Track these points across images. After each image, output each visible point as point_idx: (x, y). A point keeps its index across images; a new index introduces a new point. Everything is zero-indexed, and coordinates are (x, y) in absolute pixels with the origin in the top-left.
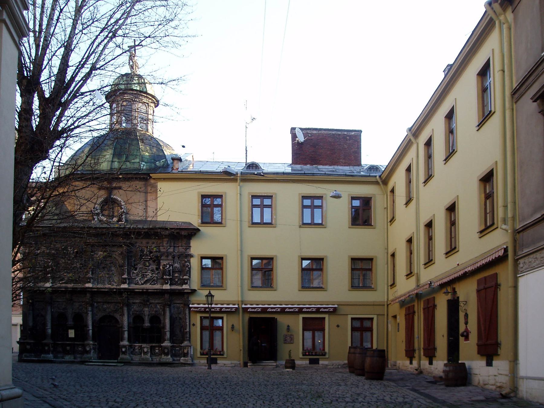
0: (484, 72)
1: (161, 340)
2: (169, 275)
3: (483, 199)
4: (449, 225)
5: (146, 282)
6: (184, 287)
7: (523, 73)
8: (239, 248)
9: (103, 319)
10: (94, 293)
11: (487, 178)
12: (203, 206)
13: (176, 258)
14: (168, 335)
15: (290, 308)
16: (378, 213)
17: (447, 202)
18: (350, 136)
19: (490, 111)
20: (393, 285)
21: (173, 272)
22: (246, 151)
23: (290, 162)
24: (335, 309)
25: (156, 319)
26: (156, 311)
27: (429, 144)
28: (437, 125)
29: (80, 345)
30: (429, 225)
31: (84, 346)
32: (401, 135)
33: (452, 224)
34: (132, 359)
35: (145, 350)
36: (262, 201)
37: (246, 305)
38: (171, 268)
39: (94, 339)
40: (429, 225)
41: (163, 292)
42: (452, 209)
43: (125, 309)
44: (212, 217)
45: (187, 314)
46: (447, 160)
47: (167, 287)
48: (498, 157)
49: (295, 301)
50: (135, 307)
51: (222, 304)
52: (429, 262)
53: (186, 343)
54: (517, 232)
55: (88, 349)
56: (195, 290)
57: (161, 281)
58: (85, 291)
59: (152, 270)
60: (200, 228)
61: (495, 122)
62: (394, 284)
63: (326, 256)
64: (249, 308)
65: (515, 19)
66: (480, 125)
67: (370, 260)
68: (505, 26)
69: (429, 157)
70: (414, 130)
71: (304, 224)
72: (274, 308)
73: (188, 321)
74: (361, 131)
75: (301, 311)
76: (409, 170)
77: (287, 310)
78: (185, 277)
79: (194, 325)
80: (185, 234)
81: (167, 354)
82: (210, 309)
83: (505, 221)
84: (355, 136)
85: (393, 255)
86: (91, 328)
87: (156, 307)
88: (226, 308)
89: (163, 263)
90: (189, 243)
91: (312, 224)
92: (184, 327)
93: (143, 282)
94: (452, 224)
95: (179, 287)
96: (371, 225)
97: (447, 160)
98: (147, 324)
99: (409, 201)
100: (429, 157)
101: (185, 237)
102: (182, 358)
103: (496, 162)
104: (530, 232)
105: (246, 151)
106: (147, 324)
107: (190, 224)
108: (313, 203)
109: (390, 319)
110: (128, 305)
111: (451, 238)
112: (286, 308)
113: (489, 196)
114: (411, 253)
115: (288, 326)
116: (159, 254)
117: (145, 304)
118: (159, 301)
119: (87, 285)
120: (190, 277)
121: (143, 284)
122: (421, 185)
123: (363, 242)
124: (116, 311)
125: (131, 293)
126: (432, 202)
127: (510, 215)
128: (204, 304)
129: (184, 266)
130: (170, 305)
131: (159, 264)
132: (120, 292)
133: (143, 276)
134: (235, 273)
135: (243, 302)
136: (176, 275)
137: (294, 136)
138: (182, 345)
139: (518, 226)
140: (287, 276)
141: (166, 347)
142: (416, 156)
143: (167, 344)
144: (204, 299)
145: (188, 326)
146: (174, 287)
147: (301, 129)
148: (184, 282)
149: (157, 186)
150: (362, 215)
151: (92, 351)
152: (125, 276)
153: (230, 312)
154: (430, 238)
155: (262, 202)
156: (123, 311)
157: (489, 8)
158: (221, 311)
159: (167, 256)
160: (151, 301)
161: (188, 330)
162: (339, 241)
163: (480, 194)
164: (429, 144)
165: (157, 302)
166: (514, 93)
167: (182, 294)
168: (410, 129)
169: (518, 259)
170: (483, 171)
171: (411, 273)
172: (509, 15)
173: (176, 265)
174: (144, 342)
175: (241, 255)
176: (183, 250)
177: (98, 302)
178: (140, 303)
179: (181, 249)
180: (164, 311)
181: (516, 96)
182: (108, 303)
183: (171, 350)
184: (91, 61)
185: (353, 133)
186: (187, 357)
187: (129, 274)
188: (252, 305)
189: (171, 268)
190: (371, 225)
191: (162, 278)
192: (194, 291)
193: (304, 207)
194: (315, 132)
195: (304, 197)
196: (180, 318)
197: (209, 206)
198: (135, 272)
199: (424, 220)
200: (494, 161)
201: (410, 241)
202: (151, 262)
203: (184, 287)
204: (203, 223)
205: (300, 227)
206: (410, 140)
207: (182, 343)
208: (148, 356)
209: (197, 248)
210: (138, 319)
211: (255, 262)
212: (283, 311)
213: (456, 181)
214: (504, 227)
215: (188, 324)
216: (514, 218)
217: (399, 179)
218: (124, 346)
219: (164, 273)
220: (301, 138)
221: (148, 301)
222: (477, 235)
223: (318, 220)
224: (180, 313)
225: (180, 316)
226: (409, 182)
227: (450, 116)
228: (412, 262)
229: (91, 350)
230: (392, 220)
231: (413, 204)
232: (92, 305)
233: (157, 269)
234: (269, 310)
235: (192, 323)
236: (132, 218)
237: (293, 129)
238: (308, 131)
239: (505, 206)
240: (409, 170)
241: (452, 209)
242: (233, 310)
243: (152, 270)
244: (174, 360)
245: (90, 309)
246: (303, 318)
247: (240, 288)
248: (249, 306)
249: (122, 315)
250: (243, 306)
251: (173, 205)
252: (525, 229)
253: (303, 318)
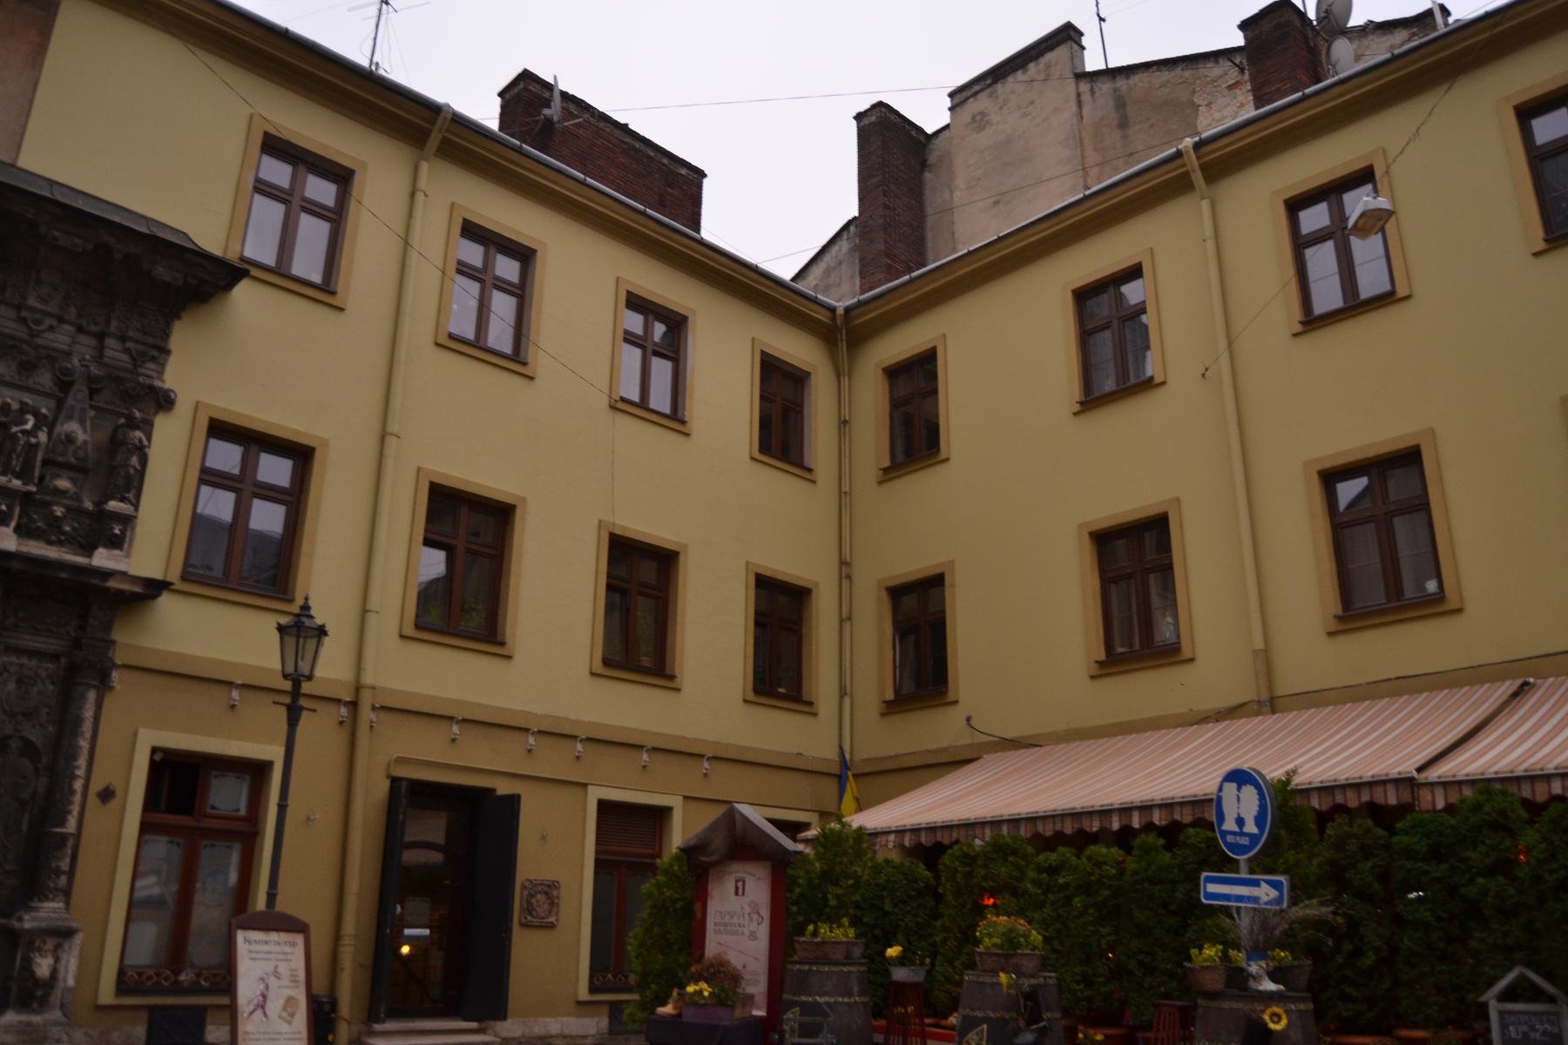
6: (102, 558)
13: (78, 395)
21: (45, 462)
38: (43, 437)
53: (49, 911)
80: (171, 281)
90: (166, 334)
109: (93, 800)
136: (63, 484)
145: (77, 798)
159: (27, 367)
173: (73, 427)
185: (684, 171)
186: (44, 1003)
193: (1301, 243)
195: (1295, 206)
203: (102, 558)
209: (231, 364)
211: (1348, 490)
223: (1371, 281)
228: (1481, 735)
235: (97, 785)
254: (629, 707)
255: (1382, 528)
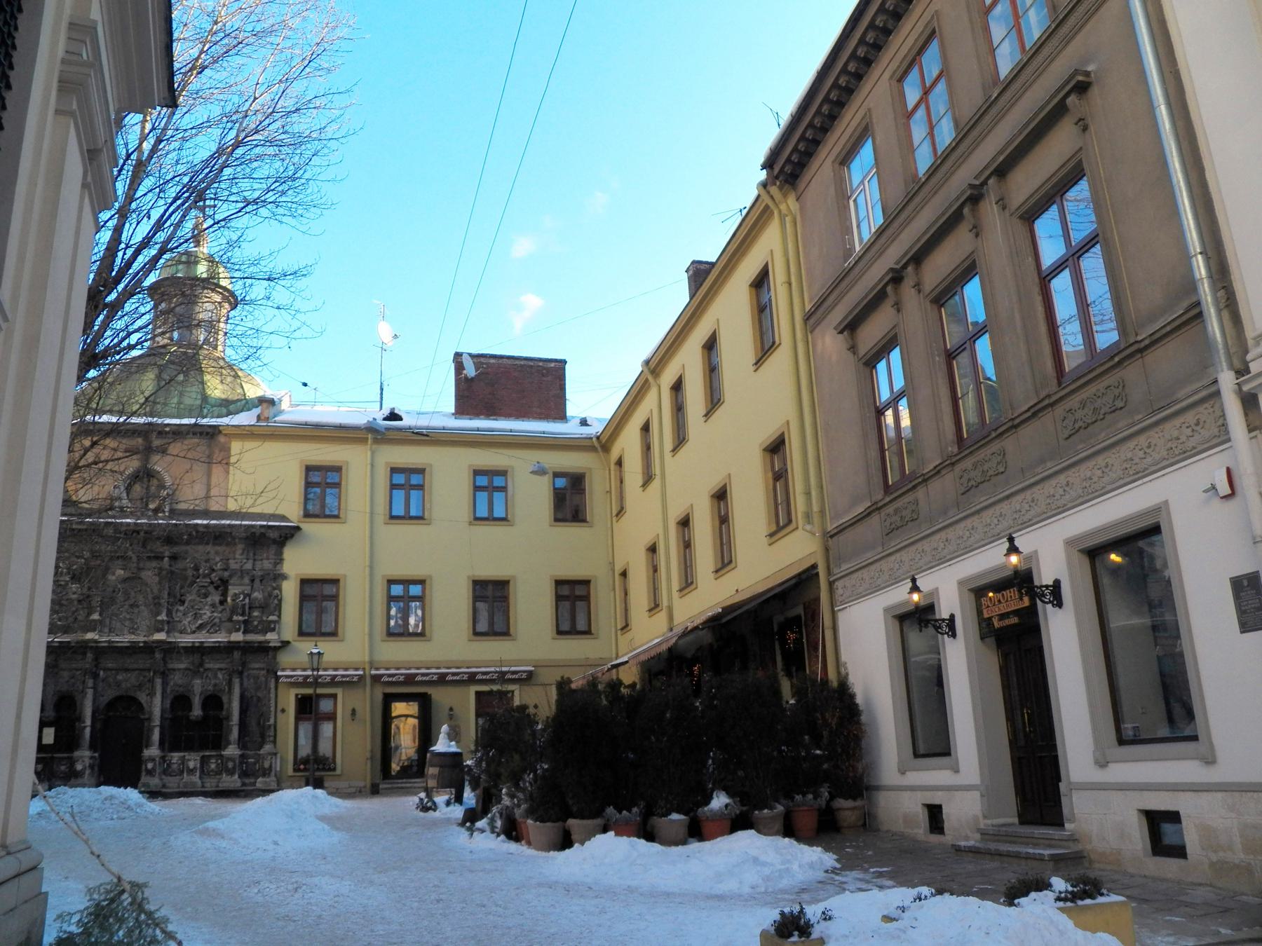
0: (761, 281)
1: (218, 743)
2: (243, 614)
3: (771, 482)
4: (717, 523)
5: (200, 627)
6: (270, 636)
7: (819, 291)
8: (367, 563)
9: (111, 705)
10: (100, 652)
11: (776, 447)
12: (308, 485)
13: (257, 582)
14: (235, 734)
15: (454, 674)
16: (597, 499)
17: (714, 484)
18: (548, 369)
19: (774, 343)
20: (626, 627)
22: (382, 389)
23: (453, 410)
24: (530, 674)
25: (213, 702)
26: (215, 685)
27: (678, 387)
28: (689, 359)
29: (63, 759)
30: (685, 523)
31: (72, 762)
32: (631, 370)
33: (723, 520)
34: (164, 786)
35: (191, 765)
36: (408, 481)
37: (377, 669)
39: (92, 747)
40: (685, 523)
41: (231, 647)
42: (721, 496)
43: (158, 681)
44: (323, 506)
45: (273, 690)
46: (708, 415)
47: (238, 637)
48: (790, 413)
49: (463, 662)
50: (177, 679)
51: (336, 669)
52: (688, 583)
53: (268, 748)
54: (829, 536)
55: (79, 767)
56: (288, 642)
57: (229, 625)
58: (83, 647)
59: (213, 605)
60: (301, 525)
61: (781, 360)
62: (627, 625)
63: (514, 577)
64: (382, 675)
65: (802, 209)
66: (759, 363)
67: (586, 583)
68: (788, 219)
69: (679, 409)
70: (652, 365)
71: (476, 519)
72: (427, 675)
73: (273, 702)
74: (565, 362)
75: (472, 679)
76: (646, 428)
77: (449, 678)
78: (271, 618)
79: (283, 711)
80: (272, 539)
81: (231, 772)
82: (316, 678)
83: (808, 516)
84: (555, 369)
85: (624, 574)
86: (88, 722)
87: (216, 677)
88: (343, 676)
89: (232, 590)
90: (281, 553)
91: (491, 519)
92: (263, 716)
93: (194, 628)
94: (723, 520)
95: (259, 638)
96: (584, 521)
97: (708, 415)
98: (197, 712)
99: (648, 479)
100: (679, 409)
101: (274, 541)
102: (260, 779)
103: (788, 422)
104: (849, 535)
105: (382, 389)
106: (197, 712)
107: (283, 518)
108: (491, 481)
110: (164, 675)
111: (722, 544)
112: (447, 674)
113: (779, 476)
114: (655, 570)
115: (451, 709)
116: (226, 574)
117: (196, 671)
118: (222, 666)
119: (90, 636)
120: (279, 616)
121: (194, 632)
122: (668, 455)
123: (572, 552)
124: (140, 687)
125: (169, 650)
126: (687, 480)
127: (816, 508)
128: (304, 670)
129: (270, 595)
130: (241, 673)
131: (224, 594)
132: (149, 648)
133: (196, 616)
134: (358, 611)
135: (372, 664)
136: (256, 614)
137: (459, 367)
138: (262, 752)
139: (830, 527)
140: (533, 609)
141: (230, 759)
142: (656, 404)
143: (232, 751)
144: (306, 659)
146: (251, 637)
147: (470, 355)
148: (269, 627)
149: (229, 449)
150: (570, 502)
151: (88, 772)
152: (163, 617)
153: (347, 684)
154: (687, 545)
155: (408, 480)
156: (153, 687)
157: (763, 193)
158: (333, 682)
159: (242, 577)
160: (207, 666)
161: (272, 721)
162: (532, 552)
163: (766, 472)
164: (678, 387)
165: (218, 666)
166: (807, 318)
167: (264, 650)
168: (647, 363)
169: (834, 581)
170: (767, 434)
171: (657, 606)
172: (791, 201)
173: (256, 594)
174: (189, 747)
175: (372, 575)
176: (270, 566)
177: (105, 670)
178: (186, 669)
179: (267, 565)
180: (230, 683)
181: (812, 321)
182: (127, 670)
183: (241, 763)
184: (161, 237)
185: (552, 365)
187: (169, 613)
188: (387, 669)
189: (247, 600)
190: (584, 521)
191: (230, 620)
192: (286, 644)
193: (477, 488)
194: (492, 361)
196: (259, 699)
197: (321, 484)
198: (181, 608)
199: (675, 514)
200: (784, 421)
201: (653, 549)
202: (211, 589)
204: (307, 515)
205: (470, 523)
206: (647, 380)
207: (261, 747)
208: (196, 778)
209: (298, 563)
210: (180, 701)
212: (442, 680)
213: (725, 448)
214: (808, 527)
215: (272, 709)
216: (822, 512)
217: (629, 442)
218: (152, 759)
219: (233, 611)
220: (470, 371)
221: (201, 665)
222: (766, 540)
223: (499, 512)
224: (258, 688)
225: (259, 694)
226: (647, 448)
227: (711, 345)
229: (84, 769)
230: (621, 512)
231: (656, 484)
232: (95, 676)
233: (222, 603)
234: (419, 678)
235: (279, 708)
236: (183, 506)
237: (458, 355)
238: (482, 360)
239: (808, 494)
240: (646, 428)
241: (721, 496)
242: (355, 679)
243: (213, 605)
244: (244, 784)
245: (90, 683)
246: (478, 694)
247: (367, 638)
248: (382, 672)
249: (152, 694)
250: (373, 672)
251: (258, 484)
252: (841, 530)
253: (478, 694)
254: (574, 649)
255: (572, 597)
